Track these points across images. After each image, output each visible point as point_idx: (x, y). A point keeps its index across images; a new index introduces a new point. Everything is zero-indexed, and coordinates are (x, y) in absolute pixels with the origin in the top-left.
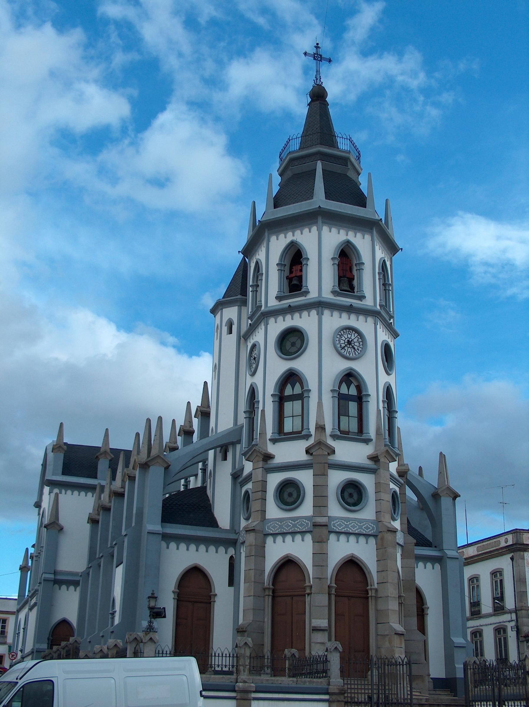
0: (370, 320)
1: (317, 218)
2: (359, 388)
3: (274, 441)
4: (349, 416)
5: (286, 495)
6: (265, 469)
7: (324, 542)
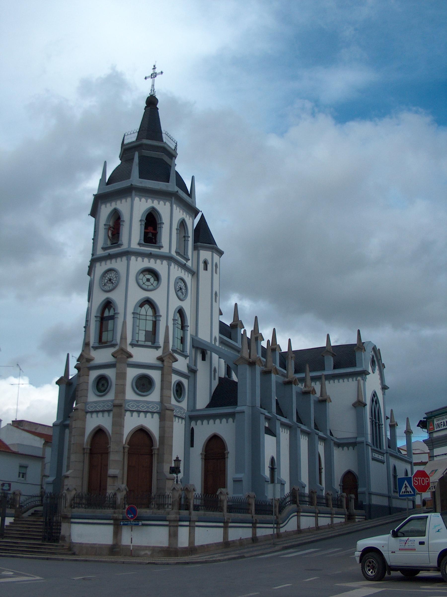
0: (165, 262)
3: (95, 348)
4: (146, 331)
5: (100, 385)
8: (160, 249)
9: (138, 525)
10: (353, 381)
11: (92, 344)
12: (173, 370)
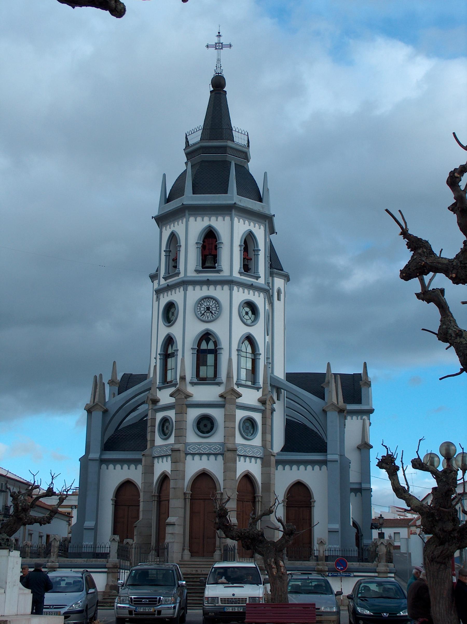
1: (185, 213)
2: (215, 343)
6: (154, 410)
7: (178, 462)
8: (257, 280)
9: (349, 576)
10: (358, 419)
11: (188, 379)
12: (237, 406)
